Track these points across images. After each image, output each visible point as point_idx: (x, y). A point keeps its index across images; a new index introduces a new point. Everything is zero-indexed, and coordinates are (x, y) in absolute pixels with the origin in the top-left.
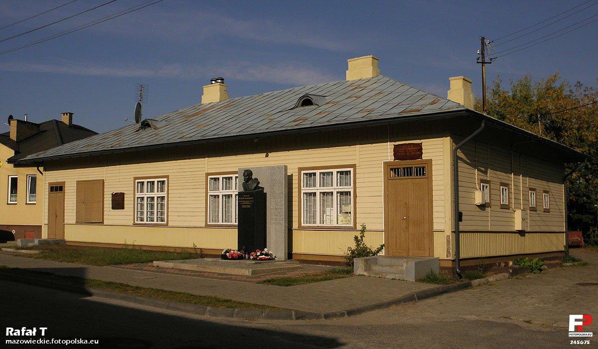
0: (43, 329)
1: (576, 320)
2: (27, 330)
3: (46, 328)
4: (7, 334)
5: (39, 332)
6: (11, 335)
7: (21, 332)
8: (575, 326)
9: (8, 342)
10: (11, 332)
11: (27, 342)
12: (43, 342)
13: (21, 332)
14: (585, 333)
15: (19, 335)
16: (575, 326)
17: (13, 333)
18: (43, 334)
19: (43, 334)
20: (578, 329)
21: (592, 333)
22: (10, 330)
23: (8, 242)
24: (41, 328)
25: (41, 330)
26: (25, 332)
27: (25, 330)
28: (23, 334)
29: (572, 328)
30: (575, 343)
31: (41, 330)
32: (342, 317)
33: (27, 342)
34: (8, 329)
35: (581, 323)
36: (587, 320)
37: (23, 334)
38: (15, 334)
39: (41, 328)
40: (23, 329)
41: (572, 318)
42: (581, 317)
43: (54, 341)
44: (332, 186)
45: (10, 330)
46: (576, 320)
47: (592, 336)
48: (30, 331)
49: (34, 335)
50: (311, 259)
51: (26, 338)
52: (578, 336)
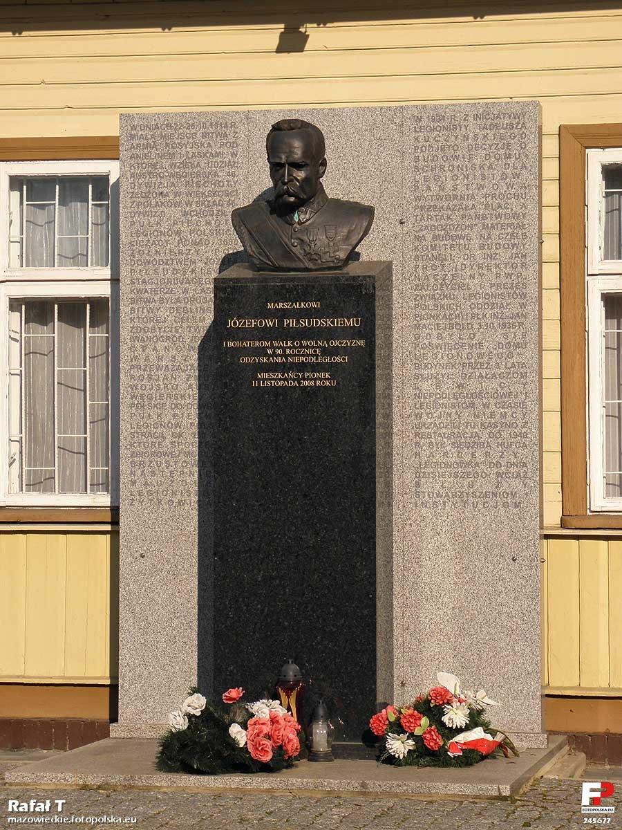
0: (60, 802)
1: (593, 790)
2: (38, 804)
3: (64, 801)
4: (10, 810)
5: (55, 806)
6: (16, 810)
7: (29, 807)
8: (590, 798)
9: (11, 820)
10: (15, 807)
11: (38, 820)
12: (60, 820)
13: (29, 807)
14: (605, 808)
15: (26, 810)
16: (590, 798)
17: (18, 807)
18: (60, 810)
19: (60, 810)
20: (594, 802)
21: (614, 808)
22: (14, 804)
23: (603, 302)
24: (56, 801)
25: (57, 804)
26: (35, 806)
27: (35, 804)
28: (32, 810)
29: (585, 801)
30: (591, 822)
31: (57, 804)
32: (88, 785)
33: (38, 820)
34: (11, 802)
35: (598, 795)
36: (607, 790)
37: (32, 810)
38: (21, 809)
39: (56, 801)
40: (32, 803)
41: (586, 787)
42: (598, 785)
43: (74, 819)
44: (87, 266)
45: (14, 804)
46: (593, 790)
47: (613, 812)
48: (42, 805)
49: (48, 810)
50: (36, 681)
51: (35, 814)
52: (595, 812)
